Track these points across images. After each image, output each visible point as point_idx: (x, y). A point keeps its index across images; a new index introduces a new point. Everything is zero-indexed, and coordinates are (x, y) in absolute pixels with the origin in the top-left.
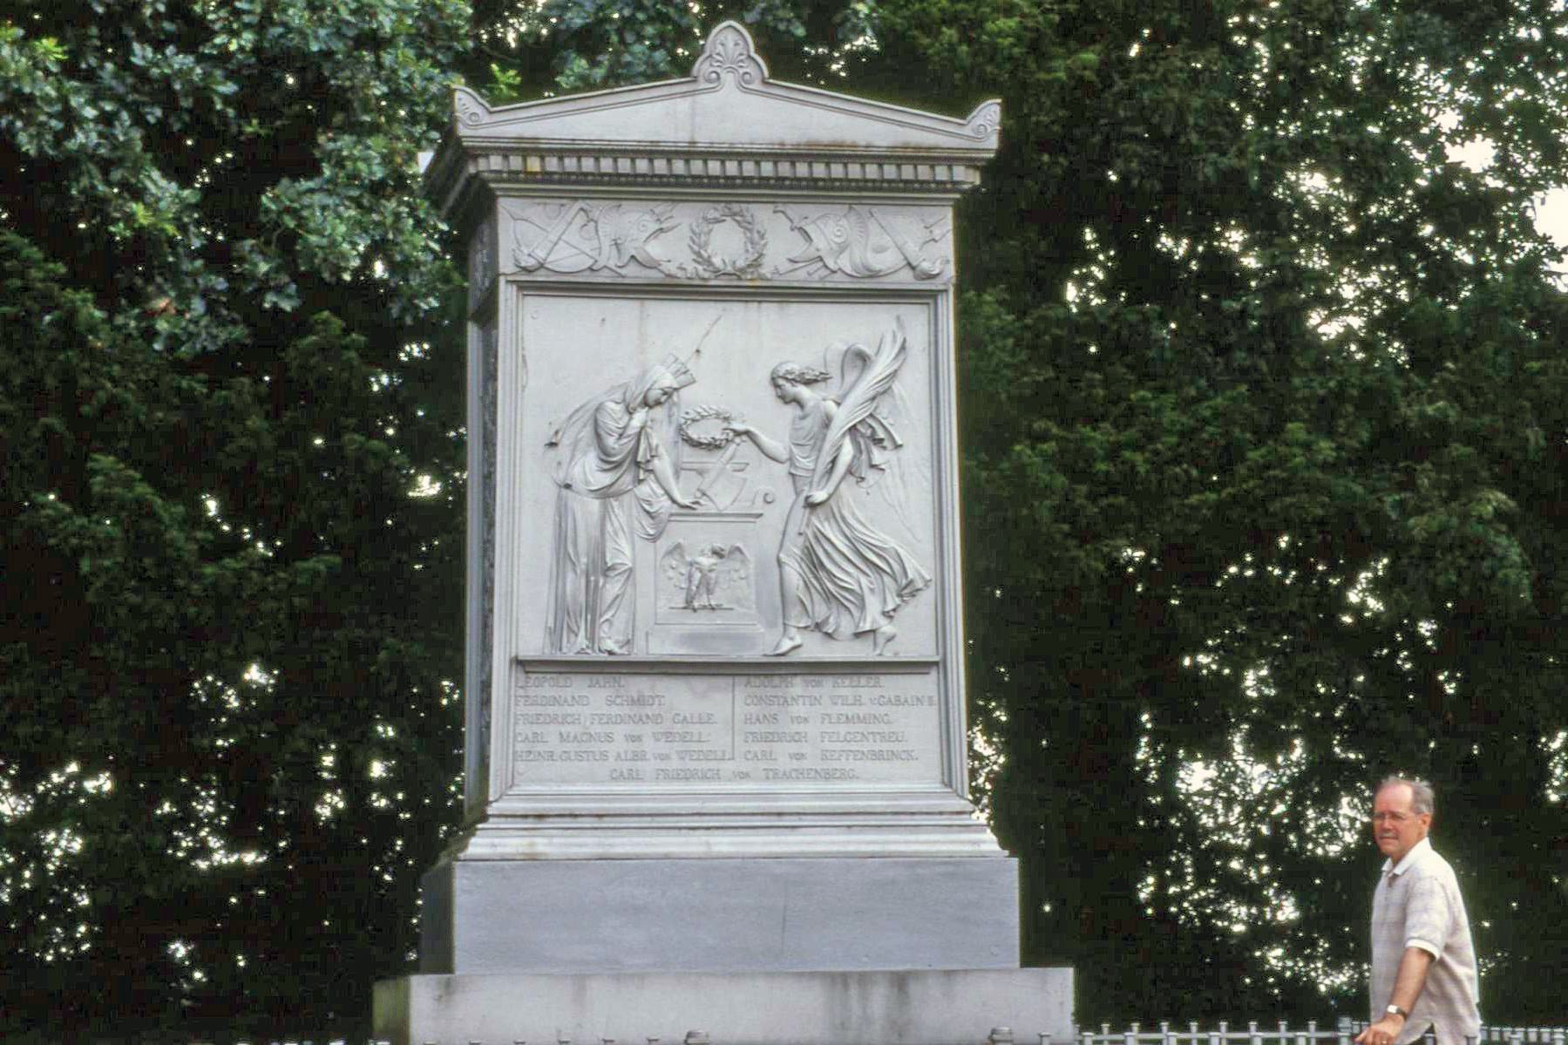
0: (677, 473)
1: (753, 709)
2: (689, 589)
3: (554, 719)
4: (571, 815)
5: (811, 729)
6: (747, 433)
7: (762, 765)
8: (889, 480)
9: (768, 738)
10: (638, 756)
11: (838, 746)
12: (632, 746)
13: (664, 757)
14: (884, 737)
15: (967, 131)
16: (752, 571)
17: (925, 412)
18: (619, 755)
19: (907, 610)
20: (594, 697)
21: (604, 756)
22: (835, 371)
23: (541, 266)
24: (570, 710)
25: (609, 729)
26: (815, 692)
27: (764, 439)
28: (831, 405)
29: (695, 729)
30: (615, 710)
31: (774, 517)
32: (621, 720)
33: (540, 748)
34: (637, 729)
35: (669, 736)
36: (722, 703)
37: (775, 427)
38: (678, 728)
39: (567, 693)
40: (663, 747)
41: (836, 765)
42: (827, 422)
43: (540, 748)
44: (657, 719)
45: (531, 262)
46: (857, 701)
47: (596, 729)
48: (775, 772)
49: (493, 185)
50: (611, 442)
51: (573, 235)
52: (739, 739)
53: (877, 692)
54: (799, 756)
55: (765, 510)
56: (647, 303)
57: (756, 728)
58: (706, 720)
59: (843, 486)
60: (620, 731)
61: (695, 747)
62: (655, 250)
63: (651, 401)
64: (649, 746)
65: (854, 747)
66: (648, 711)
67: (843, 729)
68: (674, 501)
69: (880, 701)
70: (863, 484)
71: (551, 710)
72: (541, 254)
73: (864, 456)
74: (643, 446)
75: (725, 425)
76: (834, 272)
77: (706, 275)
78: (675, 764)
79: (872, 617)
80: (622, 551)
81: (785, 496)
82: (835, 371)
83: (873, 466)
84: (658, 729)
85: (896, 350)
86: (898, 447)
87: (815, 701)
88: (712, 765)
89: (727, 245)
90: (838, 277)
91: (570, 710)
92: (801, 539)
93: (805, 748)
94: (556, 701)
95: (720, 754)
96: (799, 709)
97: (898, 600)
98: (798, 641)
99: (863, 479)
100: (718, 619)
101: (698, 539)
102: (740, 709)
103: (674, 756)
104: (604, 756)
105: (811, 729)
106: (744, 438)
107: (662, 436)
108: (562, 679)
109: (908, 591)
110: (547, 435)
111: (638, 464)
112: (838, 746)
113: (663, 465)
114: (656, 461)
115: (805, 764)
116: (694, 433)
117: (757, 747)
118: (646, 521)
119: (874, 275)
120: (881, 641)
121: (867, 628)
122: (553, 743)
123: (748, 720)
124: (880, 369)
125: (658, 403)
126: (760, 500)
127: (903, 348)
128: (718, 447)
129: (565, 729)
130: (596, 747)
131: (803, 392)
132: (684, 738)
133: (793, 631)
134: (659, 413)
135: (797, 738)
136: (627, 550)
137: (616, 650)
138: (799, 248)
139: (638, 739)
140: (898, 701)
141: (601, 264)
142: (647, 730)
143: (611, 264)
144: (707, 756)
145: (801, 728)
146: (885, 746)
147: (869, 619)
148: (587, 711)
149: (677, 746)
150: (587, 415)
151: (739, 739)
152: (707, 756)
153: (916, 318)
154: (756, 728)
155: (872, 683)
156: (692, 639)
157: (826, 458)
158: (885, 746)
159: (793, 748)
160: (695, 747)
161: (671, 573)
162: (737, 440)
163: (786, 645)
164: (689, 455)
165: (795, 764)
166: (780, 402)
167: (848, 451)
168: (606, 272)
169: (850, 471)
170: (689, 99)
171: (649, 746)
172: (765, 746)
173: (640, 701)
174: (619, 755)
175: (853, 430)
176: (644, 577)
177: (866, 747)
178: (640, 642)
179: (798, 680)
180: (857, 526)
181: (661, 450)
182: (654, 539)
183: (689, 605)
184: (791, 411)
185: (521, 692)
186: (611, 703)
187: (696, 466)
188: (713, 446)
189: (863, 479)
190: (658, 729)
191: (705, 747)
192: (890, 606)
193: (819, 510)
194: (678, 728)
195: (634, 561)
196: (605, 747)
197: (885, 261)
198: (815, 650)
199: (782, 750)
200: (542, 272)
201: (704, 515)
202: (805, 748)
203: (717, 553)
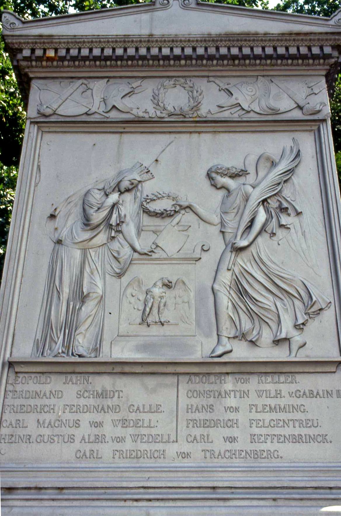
0: (139, 234)
1: (194, 402)
2: (145, 310)
3: (34, 409)
4: (36, 488)
5: (242, 417)
6: (189, 207)
7: (200, 446)
8: (294, 237)
9: (206, 424)
10: (99, 439)
11: (264, 431)
12: (96, 431)
13: (120, 440)
14: (301, 423)
15: (332, 22)
16: (192, 294)
17: (321, 229)
18: (83, 438)
19: (313, 326)
20: (68, 391)
21: (71, 439)
22: (251, 170)
23: (54, 114)
24: (47, 402)
25: (76, 417)
26: (245, 387)
27: (201, 210)
28: (249, 189)
29: (146, 417)
30: (82, 402)
31: (209, 260)
32: (88, 410)
33: (21, 432)
34: (97, 417)
35: (124, 423)
36: (168, 397)
37: (209, 202)
38: (133, 416)
39: (47, 388)
40: (119, 432)
41: (263, 446)
42: (247, 199)
43: (21, 432)
44: (116, 409)
45: (49, 111)
46: (278, 394)
47: (68, 416)
48: (212, 452)
49: (27, 70)
50: (91, 212)
51: (77, 95)
52: (182, 425)
53: (293, 387)
54: (232, 440)
55: (205, 257)
56: (125, 137)
57: (198, 416)
58: (156, 409)
59: (260, 240)
60: (86, 418)
61: (144, 431)
62: (128, 103)
63: (123, 190)
64: (108, 430)
65: (277, 431)
66: (109, 402)
67: (267, 417)
68: (135, 250)
69: (297, 394)
70: (274, 238)
71: (32, 402)
72: (55, 106)
73: (274, 220)
74: (115, 216)
75: (174, 202)
76: (248, 112)
77: (163, 115)
78: (128, 445)
79: (287, 328)
80: (97, 283)
81: (218, 246)
82: (251, 170)
83: (281, 226)
84: (117, 416)
85: (293, 156)
86: (298, 214)
87: (245, 394)
88: (160, 446)
89: (176, 98)
90: (252, 114)
91: (47, 402)
92: (230, 273)
93: (234, 432)
94: (37, 394)
95: (165, 438)
96: (231, 402)
97: (306, 317)
98: (228, 348)
99: (274, 234)
100: (167, 330)
101: (150, 273)
102: (184, 401)
103: (129, 440)
104: (71, 439)
105: (242, 417)
106: (188, 210)
107: (129, 206)
108: (43, 378)
109: (313, 310)
110: (50, 211)
111: (110, 226)
112: (264, 431)
113: (130, 229)
114: (124, 225)
115: (236, 446)
116: (154, 207)
117: (197, 432)
118: (115, 264)
119: (276, 112)
120: (294, 347)
121: (283, 336)
122: (32, 429)
123: (189, 409)
124: (282, 167)
125: (128, 190)
126: (198, 250)
127: (298, 155)
128: (171, 216)
129: (43, 417)
130: (67, 431)
131: (231, 183)
132: (136, 424)
133: (225, 340)
134: (128, 197)
135: (231, 424)
136: (100, 284)
137: (85, 354)
138: (224, 100)
139: (98, 425)
140: (312, 394)
141: (93, 110)
142: (108, 418)
143: (100, 111)
144: (155, 439)
145: (232, 416)
146: (304, 431)
147: (284, 331)
148: (60, 403)
149: (131, 431)
150: (77, 200)
151: (182, 425)
152: (155, 439)
153: (307, 143)
154: (198, 416)
155: (290, 379)
156: (144, 348)
157: (246, 219)
158: (304, 431)
159: (228, 432)
160: (144, 431)
161: (133, 300)
162: (183, 212)
163: (220, 350)
164: (146, 220)
165: (229, 446)
166: (213, 189)
167: (262, 217)
168: (97, 116)
169: (263, 229)
170: (150, 13)
171: (108, 430)
172: (205, 431)
173: (103, 394)
174: (83, 438)
175: (264, 201)
176: (111, 303)
177: (287, 431)
178: (105, 348)
179: (230, 378)
180: (273, 266)
181: (128, 218)
182: (120, 276)
183: (144, 321)
184: (221, 193)
185: (10, 388)
186: (80, 395)
187: (153, 228)
188: (162, 215)
189: (274, 234)
190: (117, 416)
191: (154, 432)
192: (300, 321)
193: (244, 255)
194: (133, 416)
195: (104, 291)
196: (71, 431)
197: (284, 104)
198: (241, 352)
199: (217, 435)
200: (53, 117)
201: (156, 259)
202: (234, 432)
203: (168, 285)
